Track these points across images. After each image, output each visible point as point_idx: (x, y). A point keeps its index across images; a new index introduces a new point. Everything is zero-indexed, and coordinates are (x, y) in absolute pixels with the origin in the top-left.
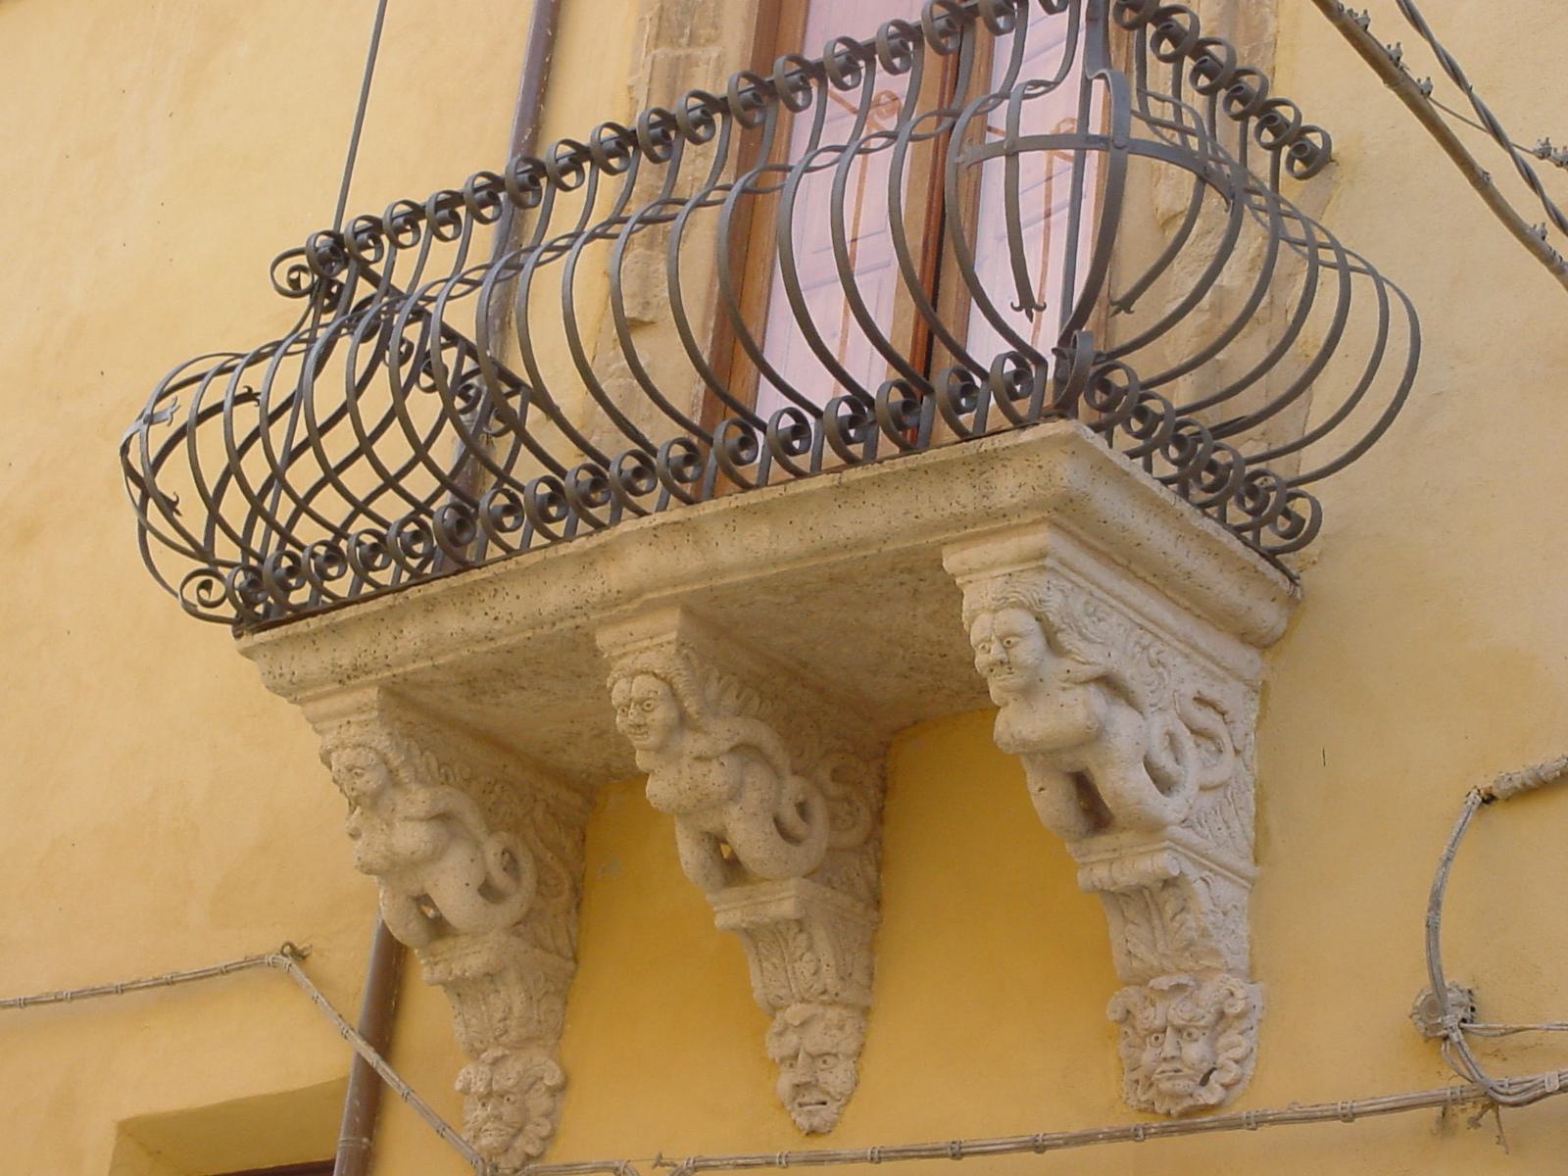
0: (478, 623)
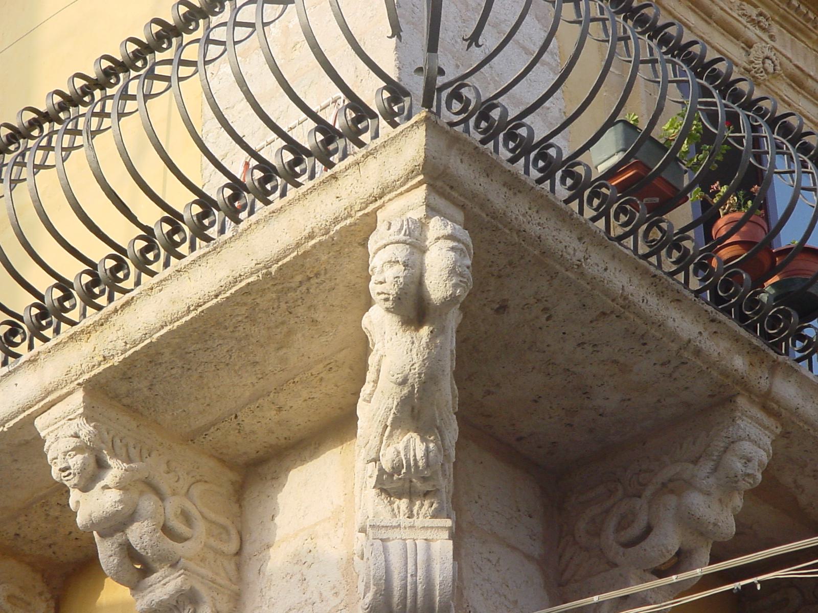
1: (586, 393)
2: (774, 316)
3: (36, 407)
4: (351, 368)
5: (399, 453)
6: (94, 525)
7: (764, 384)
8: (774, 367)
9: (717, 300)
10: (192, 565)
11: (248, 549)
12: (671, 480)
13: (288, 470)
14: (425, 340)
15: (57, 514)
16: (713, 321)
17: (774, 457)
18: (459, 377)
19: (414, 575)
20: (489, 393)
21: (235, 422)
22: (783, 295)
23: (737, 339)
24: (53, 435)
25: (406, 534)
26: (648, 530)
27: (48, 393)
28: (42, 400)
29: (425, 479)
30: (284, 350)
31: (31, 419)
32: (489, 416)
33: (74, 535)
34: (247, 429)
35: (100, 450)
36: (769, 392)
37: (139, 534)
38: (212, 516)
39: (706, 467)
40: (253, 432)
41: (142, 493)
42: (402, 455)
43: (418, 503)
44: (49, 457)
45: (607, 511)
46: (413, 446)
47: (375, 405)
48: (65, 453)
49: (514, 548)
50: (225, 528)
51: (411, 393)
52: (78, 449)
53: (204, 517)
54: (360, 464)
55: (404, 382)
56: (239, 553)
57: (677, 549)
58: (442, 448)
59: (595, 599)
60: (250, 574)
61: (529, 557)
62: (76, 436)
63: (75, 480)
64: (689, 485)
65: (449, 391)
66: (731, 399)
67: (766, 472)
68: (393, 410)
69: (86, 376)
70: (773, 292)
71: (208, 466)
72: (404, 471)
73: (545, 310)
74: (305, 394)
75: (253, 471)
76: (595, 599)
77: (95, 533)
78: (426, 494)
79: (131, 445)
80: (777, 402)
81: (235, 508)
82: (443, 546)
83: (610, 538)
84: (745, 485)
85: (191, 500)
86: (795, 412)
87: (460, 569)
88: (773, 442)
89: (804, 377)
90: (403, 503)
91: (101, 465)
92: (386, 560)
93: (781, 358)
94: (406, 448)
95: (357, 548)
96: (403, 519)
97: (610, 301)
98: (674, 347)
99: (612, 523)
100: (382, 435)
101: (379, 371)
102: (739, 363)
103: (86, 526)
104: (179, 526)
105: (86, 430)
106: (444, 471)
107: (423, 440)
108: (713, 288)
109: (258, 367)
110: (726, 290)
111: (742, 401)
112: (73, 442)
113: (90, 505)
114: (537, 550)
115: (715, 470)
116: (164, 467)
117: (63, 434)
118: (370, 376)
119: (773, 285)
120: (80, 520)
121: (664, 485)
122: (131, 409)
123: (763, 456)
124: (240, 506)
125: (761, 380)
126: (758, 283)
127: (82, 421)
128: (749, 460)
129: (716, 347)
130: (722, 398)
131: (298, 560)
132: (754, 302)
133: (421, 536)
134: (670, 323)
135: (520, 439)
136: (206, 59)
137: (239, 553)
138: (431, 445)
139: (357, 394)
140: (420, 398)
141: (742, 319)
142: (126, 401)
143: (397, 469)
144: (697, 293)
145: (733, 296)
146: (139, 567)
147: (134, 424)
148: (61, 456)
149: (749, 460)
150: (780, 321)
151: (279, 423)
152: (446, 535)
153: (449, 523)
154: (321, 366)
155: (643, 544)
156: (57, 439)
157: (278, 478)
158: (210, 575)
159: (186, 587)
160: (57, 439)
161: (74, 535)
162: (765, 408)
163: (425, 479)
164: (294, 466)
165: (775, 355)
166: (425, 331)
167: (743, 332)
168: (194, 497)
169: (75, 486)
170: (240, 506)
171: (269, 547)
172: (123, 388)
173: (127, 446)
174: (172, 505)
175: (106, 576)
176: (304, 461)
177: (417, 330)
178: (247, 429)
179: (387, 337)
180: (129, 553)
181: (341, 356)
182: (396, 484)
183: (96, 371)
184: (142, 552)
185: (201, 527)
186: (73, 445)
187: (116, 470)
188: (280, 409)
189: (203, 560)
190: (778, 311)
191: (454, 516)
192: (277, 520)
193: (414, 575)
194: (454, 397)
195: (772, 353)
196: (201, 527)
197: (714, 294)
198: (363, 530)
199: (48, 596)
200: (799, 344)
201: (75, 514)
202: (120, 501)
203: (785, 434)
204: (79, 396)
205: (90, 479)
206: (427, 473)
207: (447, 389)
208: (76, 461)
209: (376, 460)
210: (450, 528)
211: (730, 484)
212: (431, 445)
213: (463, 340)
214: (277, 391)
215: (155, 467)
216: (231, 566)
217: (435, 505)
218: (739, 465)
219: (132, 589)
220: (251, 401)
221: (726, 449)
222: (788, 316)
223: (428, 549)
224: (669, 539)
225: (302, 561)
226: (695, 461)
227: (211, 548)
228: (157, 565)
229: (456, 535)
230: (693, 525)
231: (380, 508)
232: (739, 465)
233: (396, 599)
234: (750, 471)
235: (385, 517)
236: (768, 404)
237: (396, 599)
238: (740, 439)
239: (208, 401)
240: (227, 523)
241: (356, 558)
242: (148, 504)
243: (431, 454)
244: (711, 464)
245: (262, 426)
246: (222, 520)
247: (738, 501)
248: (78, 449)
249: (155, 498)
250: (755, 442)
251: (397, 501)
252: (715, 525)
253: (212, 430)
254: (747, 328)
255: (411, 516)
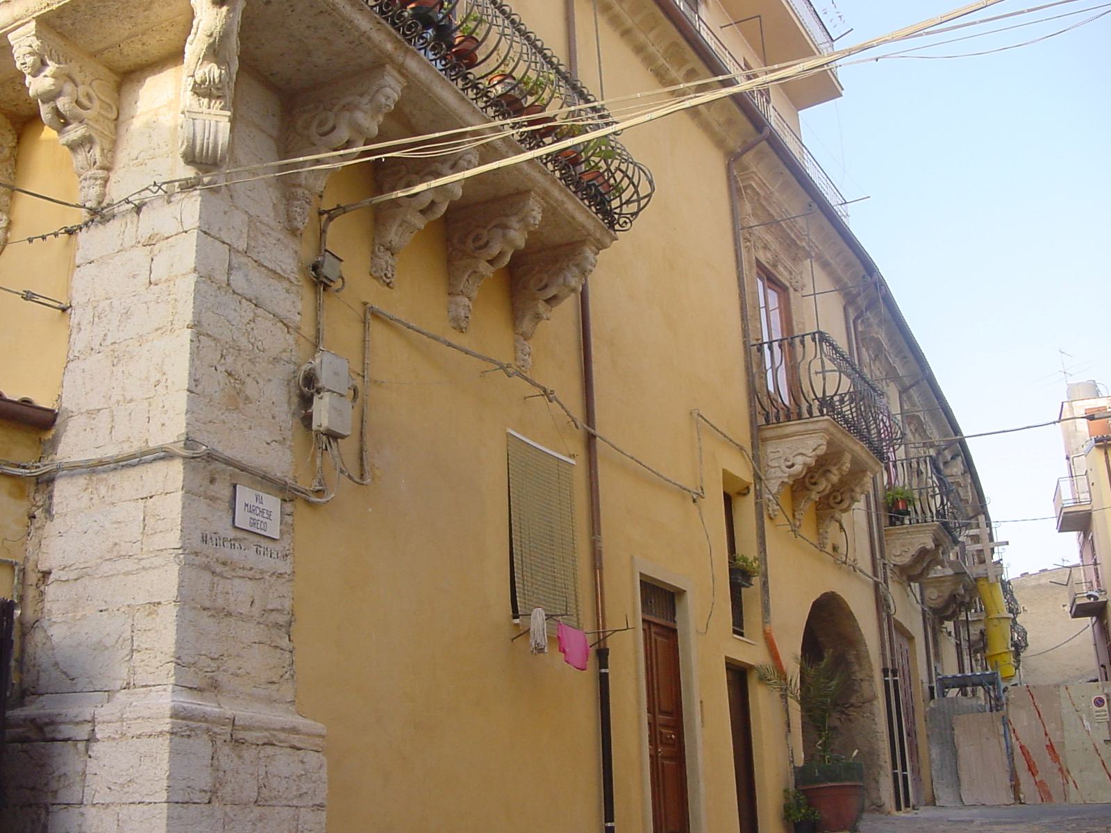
0: (843, 439)
1: (309, 54)
2: (410, 25)
3: (9, 28)
4: (184, 26)
5: (205, 74)
6: (38, 96)
7: (401, 59)
8: (407, 51)
9: (382, 12)
10: (91, 123)
11: (121, 118)
12: (348, 104)
13: (146, 78)
14: (224, 14)
15: (19, 88)
16: (379, 23)
17: (402, 98)
18: (242, 36)
19: (208, 139)
20: (257, 48)
21: (118, 48)
22: (416, 14)
23: (389, 34)
24: (18, 45)
25: (205, 117)
26: (334, 128)
27: (16, 21)
28: (13, 24)
29: (218, 89)
30: (148, 12)
31: (6, 34)
32: (257, 60)
33: (28, 101)
34: (125, 53)
35: (44, 56)
36: (403, 63)
37: (63, 103)
38: (103, 98)
39: (366, 99)
40: (128, 55)
41: (65, 81)
42: (207, 75)
43: (213, 101)
44: (15, 56)
45: (314, 117)
46: (213, 71)
47: (195, 47)
48: (24, 55)
49: (264, 132)
50: (109, 105)
51: (214, 42)
52: (31, 54)
53: (99, 98)
54: (184, 78)
55: (211, 36)
56: (116, 119)
57: (347, 139)
58: (229, 73)
59: (301, 159)
60: (122, 130)
61: (271, 136)
62: (31, 46)
63: (29, 70)
64: (357, 107)
65: (235, 43)
66: (383, 65)
67: (397, 105)
68: (204, 50)
69: (37, 14)
70: (411, 12)
71: (103, 71)
72: (207, 83)
73: (291, 6)
74: (158, 37)
75: (128, 76)
76: (301, 159)
77: (39, 101)
78: (218, 97)
79: (61, 54)
80: (407, 69)
81: (116, 95)
82: (225, 125)
83: (313, 130)
84: (385, 110)
85: (92, 88)
86: (414, 75)
87: (233, 139)
88: (402, 91)
89: (422, 59)
90: (206, 101)
91: (44, 64)
92: (194, 130)
93: (411, 47)
94: (210, 71)
95: (180, 122)
96: (204, 109)
97: (325, 6)
98: (357, 34)
99: (315, 123)
100: (197, 63)
101: (198, 28)
102: (389, 47)
103: (34, 96)
104: (85, 102)
105: (36, 43)
106: (229, 87)
107: (219, 68)
108: (380, 5)
109: (132, 20)
110: (387, 8)
111: (388, 67)
112: (29, 49)
113: (37, 85)
114: (275, 133)
115: (371, 101)
116: (78, 69)
117: (24, 44)
118: (193, 31)
119: (412, 9)
120: (31, 93)
121: (344, 106)
122: (61, 35)
123: (396, 97)
124: (119, 95)
125: (400, 57)
126: (404, 6)
127: (34, 38)
128: (389, 98)
129: (378, 37)
130: (379, 64)
131: (148, 125)
132: (400, 16)
133: (214, 119)
134: (356, 21)
135: (272, 74)
136: (652, 625)
137: (116, 119)
138: (223, 71)
139: (186, 41)
140: (219, 45)
141: (393, 24)
142: (59, 30)
143: (203, 82)
144: (372, 7)
145: (390, 11)
146: (62, 121)
147: (63, 43)
148: (22, 56)
149: (389, 98)
150: (412, 27)
151: (143, 52)
152: (227, 119)
153: (229, 113)
154: (167, 23)
155: (331, 135)
156: (20, 47)
157: (140, 81)
158: (100, 129)
159: (87, 134)
160: (20, 47)
161: (28, 101)
162: (400, 72)
163: (218, 89)
164: (149, 76)
165: (408, 45)
166: (225, 9)
167: (393, 31)
168: (95, 87)
169: (29, 74)
170: (119, 95)
171: (133, 117)
172: (58, 22)
173: (58, 55)
174: (82, 90)
175: (44, 125)
176: (155, 74)
177: (220, 8)
178: (125, 53)
179: (204, 10)
180: (57, 113)
181: (179, 18)
182: (203, 90)
183: (43, 11)
184: (64, 113)
185: (97, 103)
186: (28, 51)
187: (52, 67)
188: (143, 44)
189: (97, 121)
190: (413, 23)
191: (232, 110)
192: (138, 103)
193: (208, 139)
194: (237, 47)
195: (406, 43)
196: (97, 103)
197: (381, 9)
198: (183, 113)
199: (14, 132)
200: (421, 41)
201: (28, 89)
202: (53, 84)
203: (408, 87)
204: (33, 24)
205: (38, 70)
206: (219, 86)
207: (234, 43)
208: (30, 60)
209: (193, 76)
210: (229, 117)
211: (378, 109)
212: (223, 71)
213: (245, 16)
214: (143, 34)
215: (73, 68)
216: (112, 126)
217: (223, 104)
218: (383, 100)
219: (58, 132)
220: (128, 38)
221: (377, 91)
222: (417, 26)
223: (217, 126)
224: (344, 134)
225: (151, 126)
226: (361, 95)
227: (102, 115)
228: (71, 121)
229: (233, 121)
230: (357, 128)
231: (193, 102)
232: (383, 100)
233: (198, 149)
234: (388, 103)
235: (196, 108)
236: (402, 70)
237: (198, 149)
238: (385, 86)
239: (104, 35)
240: (112, 103)
241: (179, 128)
242: (69, 87)
243: (223, 77)
244: (369, 97)
245: (134, 52)
246: (108, 101)
247: (381, 118)
248: (31, 54)
249: (72, 85)
250: (392, 88)
251: (203, 99)
252: (368, 129)
253: (106, 51)
254: (395, 29)
255: (209, 108)
